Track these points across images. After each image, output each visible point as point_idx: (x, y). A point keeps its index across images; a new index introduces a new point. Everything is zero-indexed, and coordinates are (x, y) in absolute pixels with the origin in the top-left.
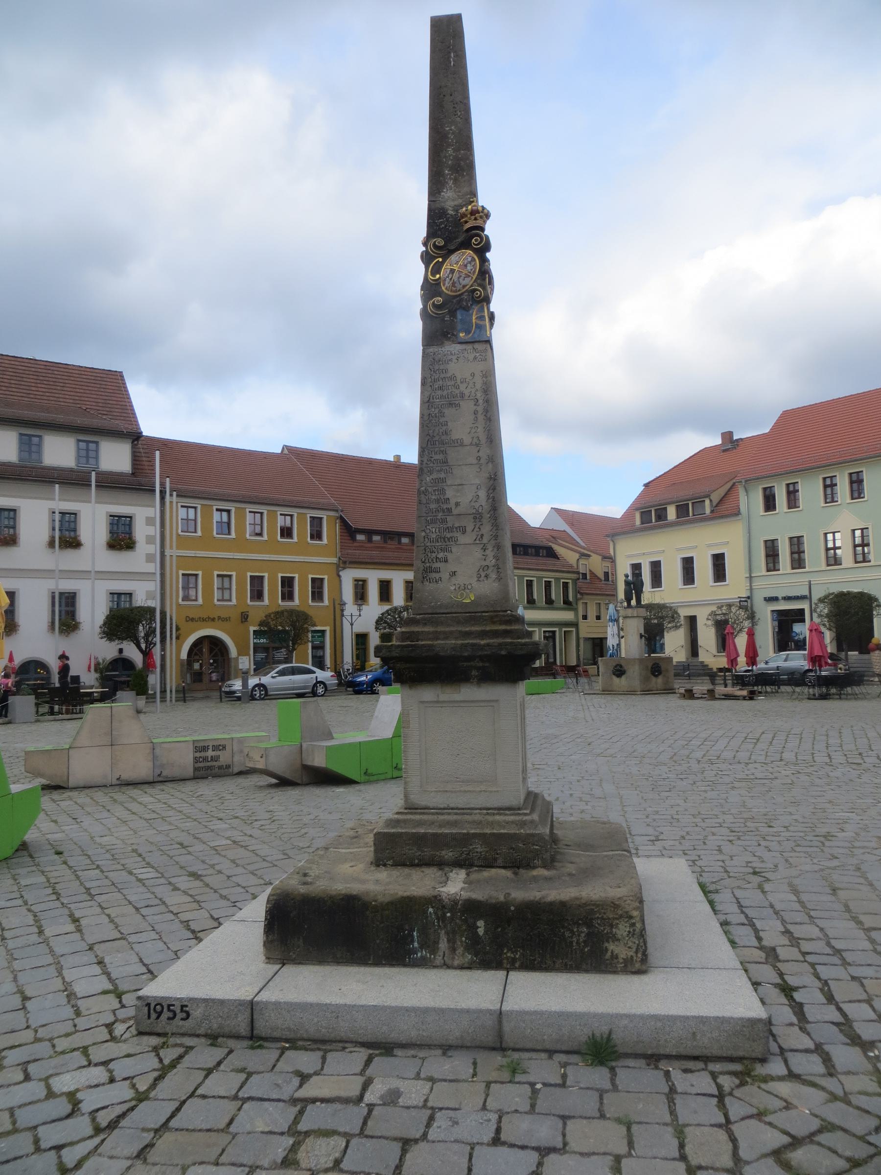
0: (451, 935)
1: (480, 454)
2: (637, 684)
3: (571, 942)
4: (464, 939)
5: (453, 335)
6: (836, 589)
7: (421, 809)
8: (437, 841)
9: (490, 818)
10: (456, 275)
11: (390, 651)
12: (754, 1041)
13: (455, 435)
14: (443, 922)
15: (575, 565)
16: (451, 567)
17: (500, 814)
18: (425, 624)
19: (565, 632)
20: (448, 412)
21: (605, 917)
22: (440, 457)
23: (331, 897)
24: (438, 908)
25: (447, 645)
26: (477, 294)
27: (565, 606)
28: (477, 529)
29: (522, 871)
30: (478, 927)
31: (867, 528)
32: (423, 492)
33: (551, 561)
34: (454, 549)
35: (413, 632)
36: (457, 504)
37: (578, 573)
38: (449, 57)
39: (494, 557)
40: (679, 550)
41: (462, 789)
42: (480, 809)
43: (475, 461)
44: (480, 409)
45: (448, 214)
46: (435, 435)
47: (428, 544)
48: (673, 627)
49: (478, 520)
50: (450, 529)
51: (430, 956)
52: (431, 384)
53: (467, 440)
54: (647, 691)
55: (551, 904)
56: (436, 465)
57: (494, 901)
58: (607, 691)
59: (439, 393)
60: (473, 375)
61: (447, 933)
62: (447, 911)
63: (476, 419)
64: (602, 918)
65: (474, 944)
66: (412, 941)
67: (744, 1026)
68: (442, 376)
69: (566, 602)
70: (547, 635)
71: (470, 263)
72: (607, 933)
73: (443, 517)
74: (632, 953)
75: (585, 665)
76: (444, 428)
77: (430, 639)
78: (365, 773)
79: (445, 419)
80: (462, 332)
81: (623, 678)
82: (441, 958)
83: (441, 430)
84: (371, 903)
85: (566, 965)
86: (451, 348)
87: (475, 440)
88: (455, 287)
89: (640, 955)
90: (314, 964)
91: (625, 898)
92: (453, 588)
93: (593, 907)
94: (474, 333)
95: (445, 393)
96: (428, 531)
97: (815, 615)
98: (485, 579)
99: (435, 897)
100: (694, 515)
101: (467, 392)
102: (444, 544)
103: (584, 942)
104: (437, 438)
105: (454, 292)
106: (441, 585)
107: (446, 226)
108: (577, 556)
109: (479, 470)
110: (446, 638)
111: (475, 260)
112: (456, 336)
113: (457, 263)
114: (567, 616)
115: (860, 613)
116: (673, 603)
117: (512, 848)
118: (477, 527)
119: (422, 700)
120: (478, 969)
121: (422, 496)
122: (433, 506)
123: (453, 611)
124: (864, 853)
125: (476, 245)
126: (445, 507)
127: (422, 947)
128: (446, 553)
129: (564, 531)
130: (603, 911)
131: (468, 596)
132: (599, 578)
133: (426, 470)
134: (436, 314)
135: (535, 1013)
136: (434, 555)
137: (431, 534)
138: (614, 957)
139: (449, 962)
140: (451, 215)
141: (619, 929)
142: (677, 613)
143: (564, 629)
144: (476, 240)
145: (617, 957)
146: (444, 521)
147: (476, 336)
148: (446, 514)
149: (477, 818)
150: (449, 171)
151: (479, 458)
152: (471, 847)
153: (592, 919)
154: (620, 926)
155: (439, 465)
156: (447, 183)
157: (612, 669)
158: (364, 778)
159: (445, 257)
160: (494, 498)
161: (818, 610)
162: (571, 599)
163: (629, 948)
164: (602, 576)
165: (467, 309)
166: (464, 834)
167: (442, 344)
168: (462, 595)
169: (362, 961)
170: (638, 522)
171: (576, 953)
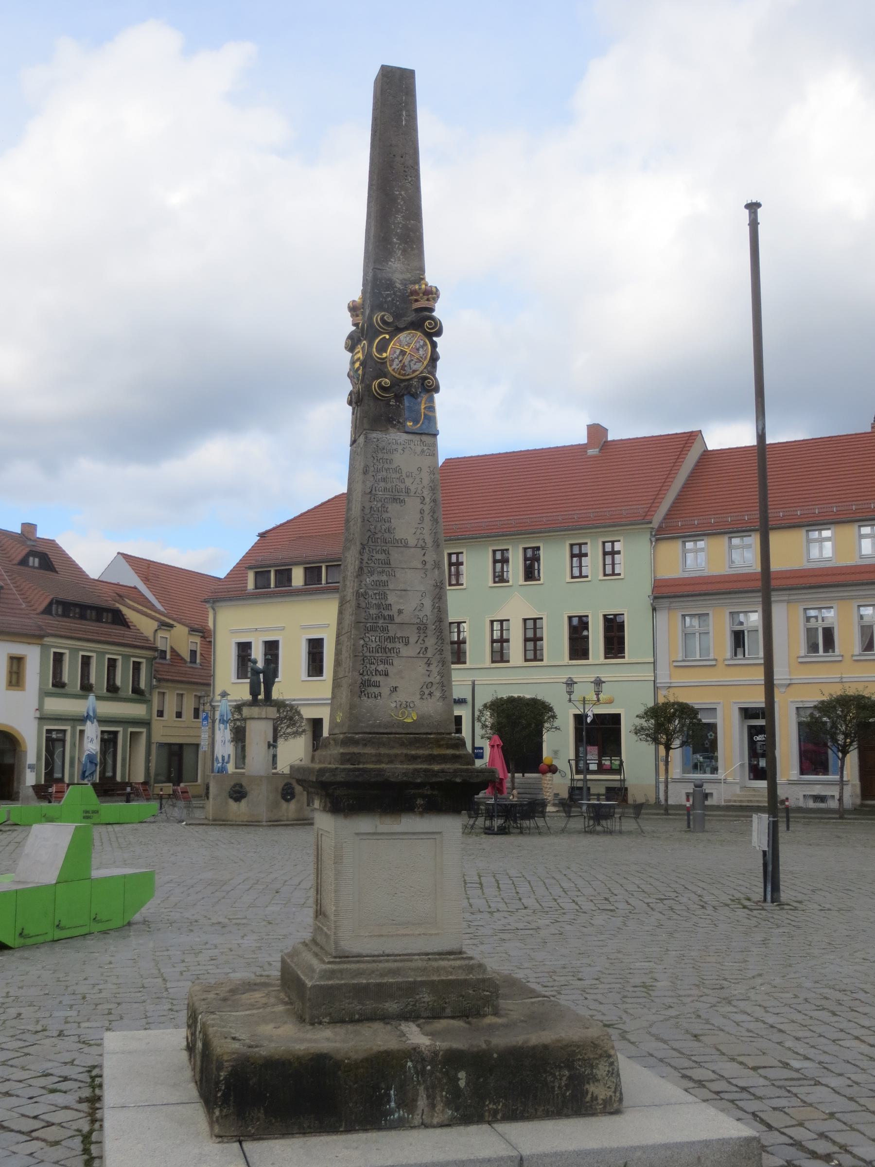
0: (430, 1090)
1: (426, 558)
2: (263, 813)
3: (553, 1087)
4: (444, 1093)
5: (399, 422)
6: (504, 694)
7: (353, 957)
8: (381, 991)
9: (435, 964)
10: (406, 359)
11: (334, 775)
12: (749, 1159)
13: (400, 534)
14: (423, 1076)
15: (151, 639)
16: (392, 682)
17: (443, 960)
18: (365, 745)
19: (132, 733)
20: (393, 507)
21: (586, 1057)
22: (382, 556)
23: (298, 1058)
24: (417, 1062)
25: (398, 769)
26: (429, 382)
27: (135, 696)
28: (420, 641)
29: (474, 1021)
30: (459, 1079)
31: (541, 618)
32: (362, 595)
33: (118, 630)
34: (396, 662)
35: (354, 753)
36: (400, 612)
37: (155, 649)
38: (401, 115)
39: (439, 673)
40: (304, 628)
41: (399, 932)
42: (419, 954)
43: (420, 566)
44: (427, 508)
45: (396, 287)
46: (377, 531)
47: (368, 654)
48: (294, 733)
49: (422, 631)
50: (392, 639)
51: (408, 1116)
52: (374, 474)
53: (412, 542)
54: (275, 823)
55: (534, 1048)
56: (377, 565)
57: (475, 1049)
58: (220, 822)
59: (382, 484)
60: (420, 469)
61: (427, 1089)
62: (427, 1063)
63: (422, 519)
64: (583, 1060)
65: (455, 1099)
66: (389, 1102)
67: (742, 1146)
68: (386, 466)
69: (136, 690)
70: (106, 737)
71: (422, 347)
72: (588, 1074)
73: (384, 625)
74: (611, 1093)
75: (156, 782)
76: (387, 525)
77: (372, 763)
78: (20, 934)
79: (388, 515)
80: (410, 421)
81: (244, 802)
82: (419, 1116)
83: (383, 527)
84: (344, 1061)
85: (548, 1111)
86: (395, 436)
87: (421, 542)
88: (404, 370)
89: (618, 1094)
90: (276, 1138)
91: (602, 1037)
92: (393, 705)
93: (575, 1049)
94: (423, 423)
95: (389, 486)
96: (367, 639)
97: (478, 725)
98: (429, 697)
99: (414, 1049)
100: (327, 583)
101: (413, 488)
102: (385, 655)
103: (566, 1085)
104: (379, 535)
105: (402, 375)
106: (380, 701)
107: (393, 300)
108: (155, 625)
109: (424, 576)
110: (391, 762)
111: (427, 345)
112: (403, 425)
113: (408, 344)
114: (137, 710)
115: (533, 725)
116: (294, 700)
117: (461, 996)
118: (421, 638)
119: (357, 831)
120: (460, 1124)
121: (362, 599)
122: (373, 611)
123: (394, 730)
124: (692, 1001)
125: (430, 329)
126: (386, 614)
127: (399, 1106)
128: (386, 666)
129: (135, 588)
130: (584, 1052)
131: (409, 715)
132: (182, 659)
133: (365, 570)
134: (376, 391)
135: (556, 1154)
136: (373, 667)
137: (370, 643)
138: (594, 1098)
139: (427, 1120)
140: (399, 289)
141: (599, 1070)
142: (299, 713)
143: (130, 730)
144: (430, 324)
145: (596, 1099)
146: (385, 629)
147: (424, 427)
148: (386, 621)
149: (420, 964)
150: (397, 239)
151: (424, 563)
152: (418, 997)
153: (574, 1061)
154: (600, 1066)
155: (380, 565)
156: (395, 252)
157: (228, 789)
158: (18, 942)
159: (393, 335)
160: (439, 608)
161: (483, 719)
162: (142, 685)
163: (609, 1087)
164: (187, 656)
165: (415, 396)
166: (410, 983)
167: (386, 431)
168: (403, 713)
169: (333, 1130)
170: (251, 585)
171: (558, 1097)
